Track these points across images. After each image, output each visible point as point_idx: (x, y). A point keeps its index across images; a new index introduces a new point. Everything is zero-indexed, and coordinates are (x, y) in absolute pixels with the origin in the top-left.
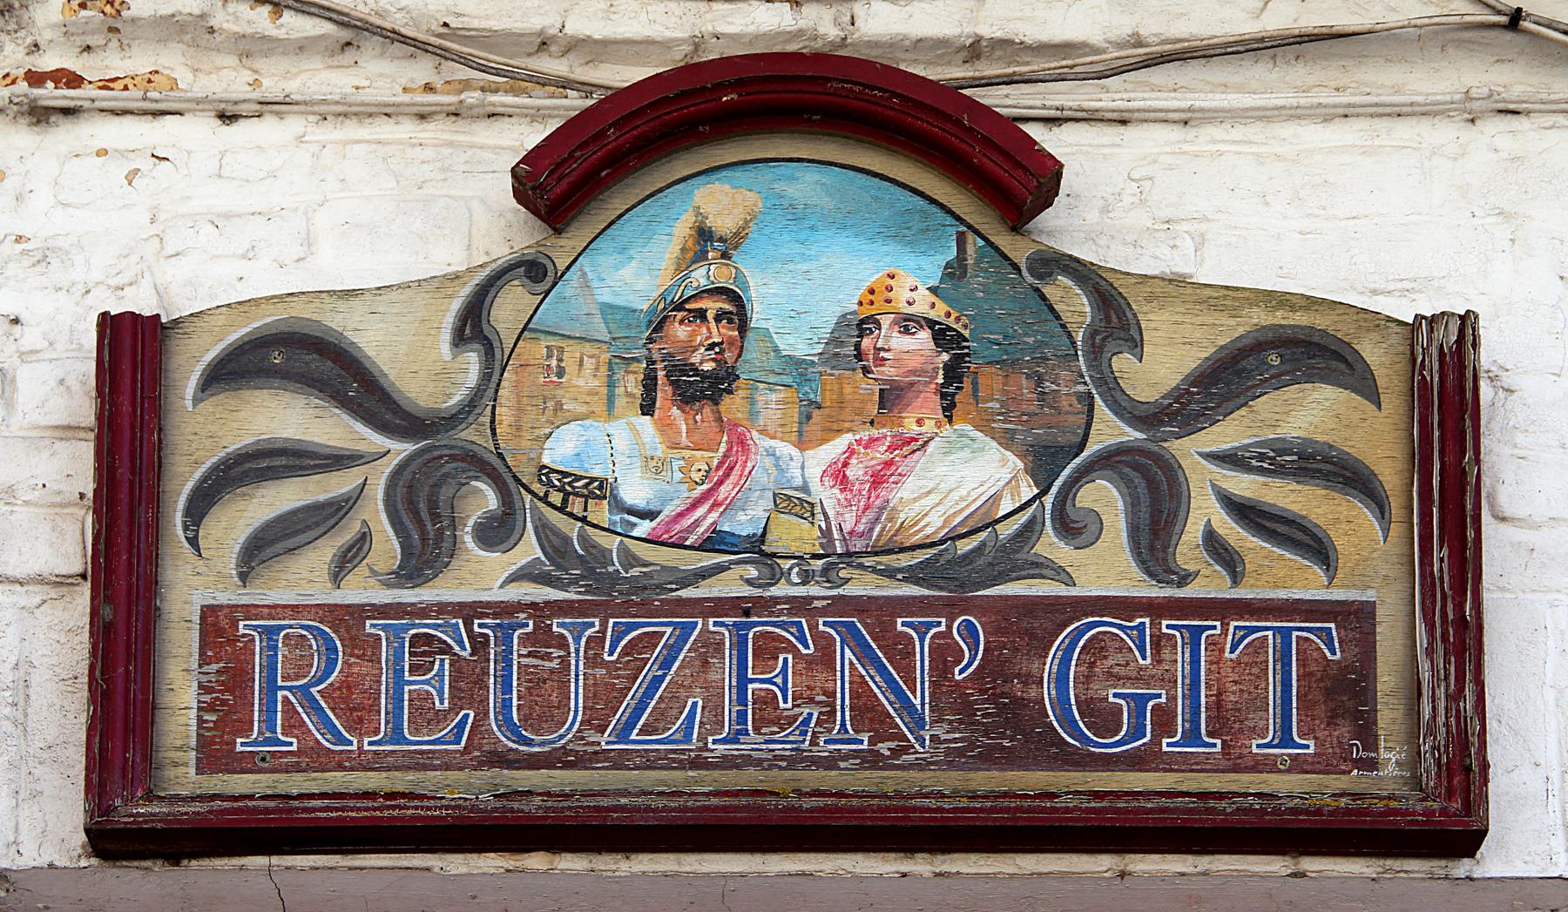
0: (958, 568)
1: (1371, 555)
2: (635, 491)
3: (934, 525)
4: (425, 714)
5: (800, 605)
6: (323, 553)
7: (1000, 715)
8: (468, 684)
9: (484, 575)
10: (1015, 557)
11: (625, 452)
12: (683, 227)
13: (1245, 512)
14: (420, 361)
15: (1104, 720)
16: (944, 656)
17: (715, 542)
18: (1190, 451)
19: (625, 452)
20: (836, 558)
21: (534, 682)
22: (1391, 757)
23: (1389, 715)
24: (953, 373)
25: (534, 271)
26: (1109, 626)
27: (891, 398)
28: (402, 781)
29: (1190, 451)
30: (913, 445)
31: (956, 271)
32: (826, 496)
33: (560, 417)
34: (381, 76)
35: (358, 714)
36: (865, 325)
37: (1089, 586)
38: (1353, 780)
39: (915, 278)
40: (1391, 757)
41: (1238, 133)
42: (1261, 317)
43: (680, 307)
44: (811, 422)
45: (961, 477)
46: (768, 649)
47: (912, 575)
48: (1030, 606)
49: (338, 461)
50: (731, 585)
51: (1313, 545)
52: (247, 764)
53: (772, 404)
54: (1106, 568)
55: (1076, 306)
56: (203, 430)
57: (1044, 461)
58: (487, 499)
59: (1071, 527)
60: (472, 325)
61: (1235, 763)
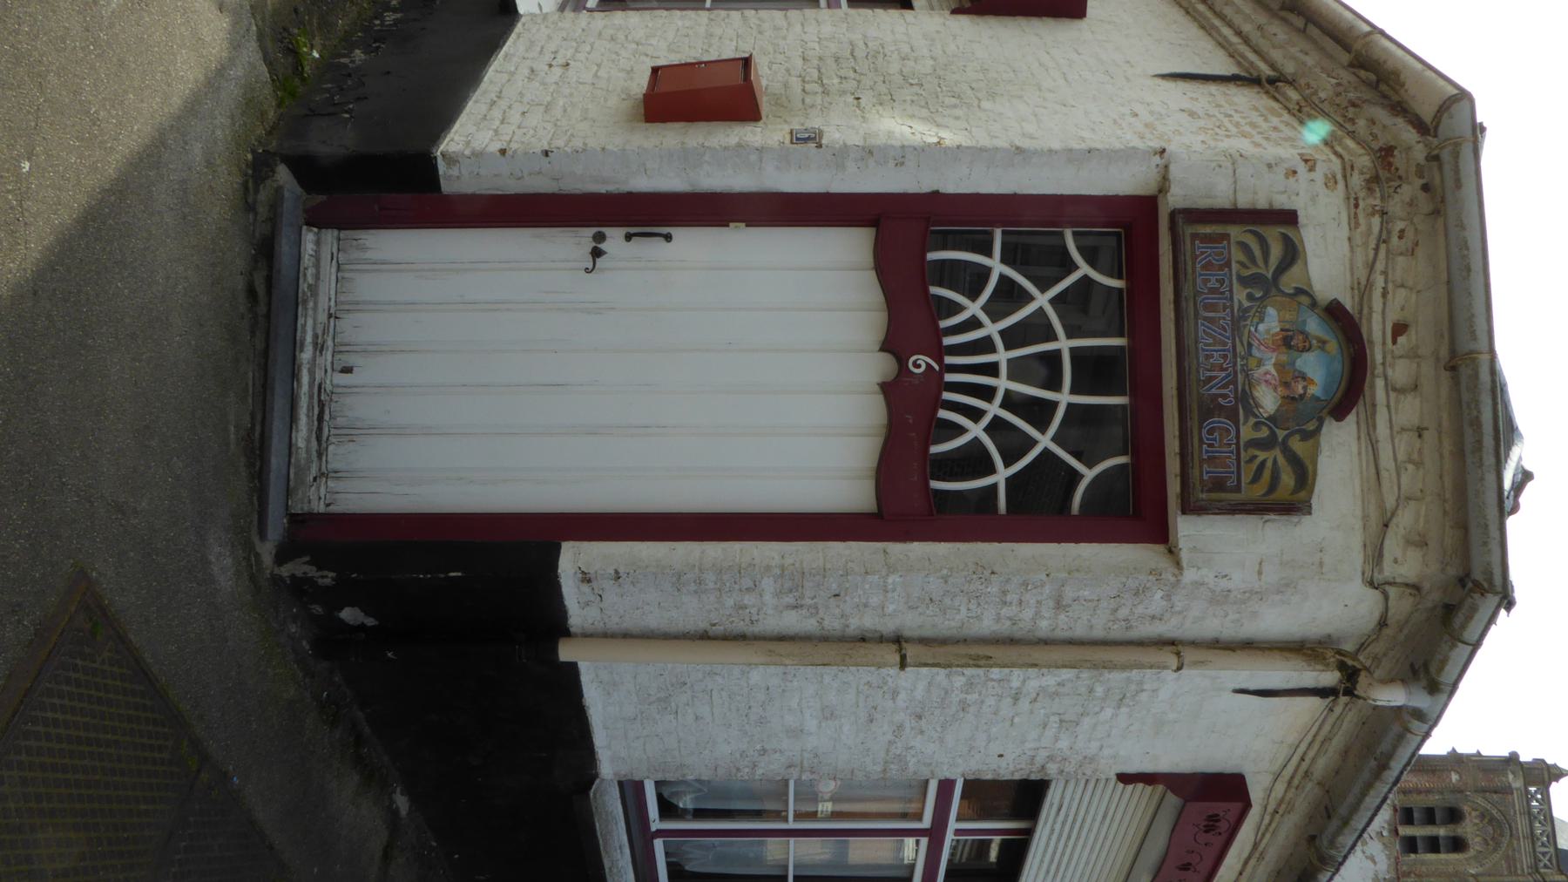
0: (1246, 400)
1: (1257, 492)
2: (1261, 327)
3: (1256, 394)
4: (1206, 281)
5: (1235, 364)
6: (1242, 258)
7: (1210, 409)
8: (1213, 291)
9: (1240, 295)
10: (1250, 412)
11: (1271, 322)
12: (1326, 338)
13: (1263, 463)
14: (1289, 281)
15: (1211, 432)
16: (1225, 396)
17: (1250, 345)
18: (1277, 452)
19: (1271, 322)
20: (1247, 373)
21: (1212, 305)
22: (1204, 496)
23: (1214, 496)
24: (1293, 399)
25: (1314, 304)
26: (1233, 433)
27: (1286, 385)
28: (1190, 277)
29: (1277, 452)
30: (1275, 389)
31: (1318, 399)
32: (1262, 370)
33: (1279, 311)
34: (1362, 274)
35: (1204, 267)
36: (1304, 378)
37: (1242, 429)
38: (1198, 486)
39: (1314, 390)
40: (1204, 496)
41: (1035, 681)
42: (1310, 468)
43: (1306, 336)
44: (1279, 366)
45: (1268, 400)
46: (1225, 357)
47: (1243, 390)
48: (1237, 414)
49: (1266, 261)
50: (1239, 348)
51: (1257, 478)
52: (1193, 243)
53: (1284, 358)
54: (1247, 432)
55: (1311, 427)
56: (1273, 234)
57: (1270, 418)
58: (1258, 295)
59: (1257, 426)
60: (1299, 291)
61: (1202, 461)
